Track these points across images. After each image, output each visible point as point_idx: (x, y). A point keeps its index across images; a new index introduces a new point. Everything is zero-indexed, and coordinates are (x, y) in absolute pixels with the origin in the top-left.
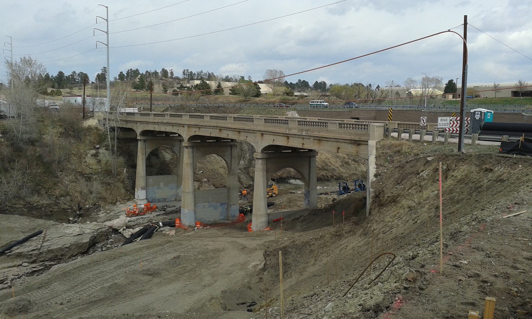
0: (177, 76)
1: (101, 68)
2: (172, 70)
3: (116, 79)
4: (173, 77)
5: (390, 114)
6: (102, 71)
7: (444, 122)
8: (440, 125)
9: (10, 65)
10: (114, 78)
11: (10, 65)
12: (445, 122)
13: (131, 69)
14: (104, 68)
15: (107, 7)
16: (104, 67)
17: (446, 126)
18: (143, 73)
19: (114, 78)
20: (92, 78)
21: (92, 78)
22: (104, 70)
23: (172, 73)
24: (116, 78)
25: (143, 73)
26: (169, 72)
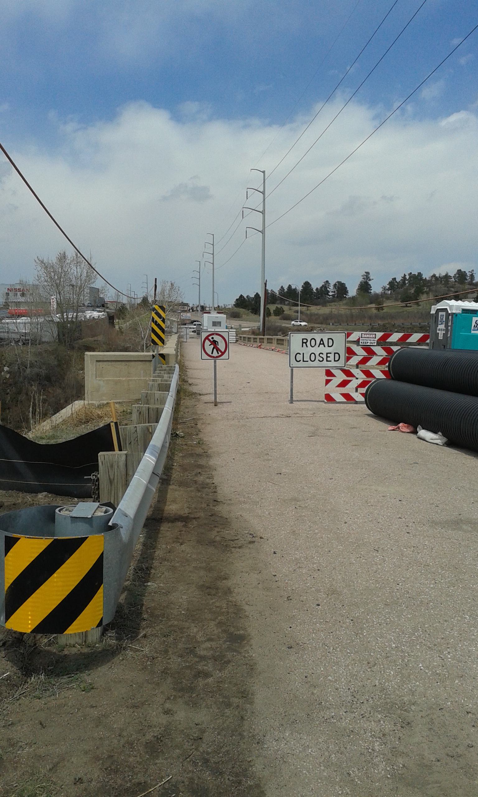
0: (359, 283)
1: (362, 274)
2: (473, 270)
3: (384, 288)
4: (474, 282)
5: (156, 323)
6: (363, 278)
7: (317, 350)
8: (299, 357)
9: (447, 274)
10: (382, 288)
11: (447, 274)
12: (325, 350)
13: (411, 273)
14: (366, 274)
15: (213, 235)
16: (366, 272)
17: (333, 364)
18: (426, 278)
19: (382, 288)
20: (352, 291)
21: (352, 291)
22: (366, 276)
23: (472, 276)
24: (385, 288)
25: (426, 278)
26: (468, 274)
